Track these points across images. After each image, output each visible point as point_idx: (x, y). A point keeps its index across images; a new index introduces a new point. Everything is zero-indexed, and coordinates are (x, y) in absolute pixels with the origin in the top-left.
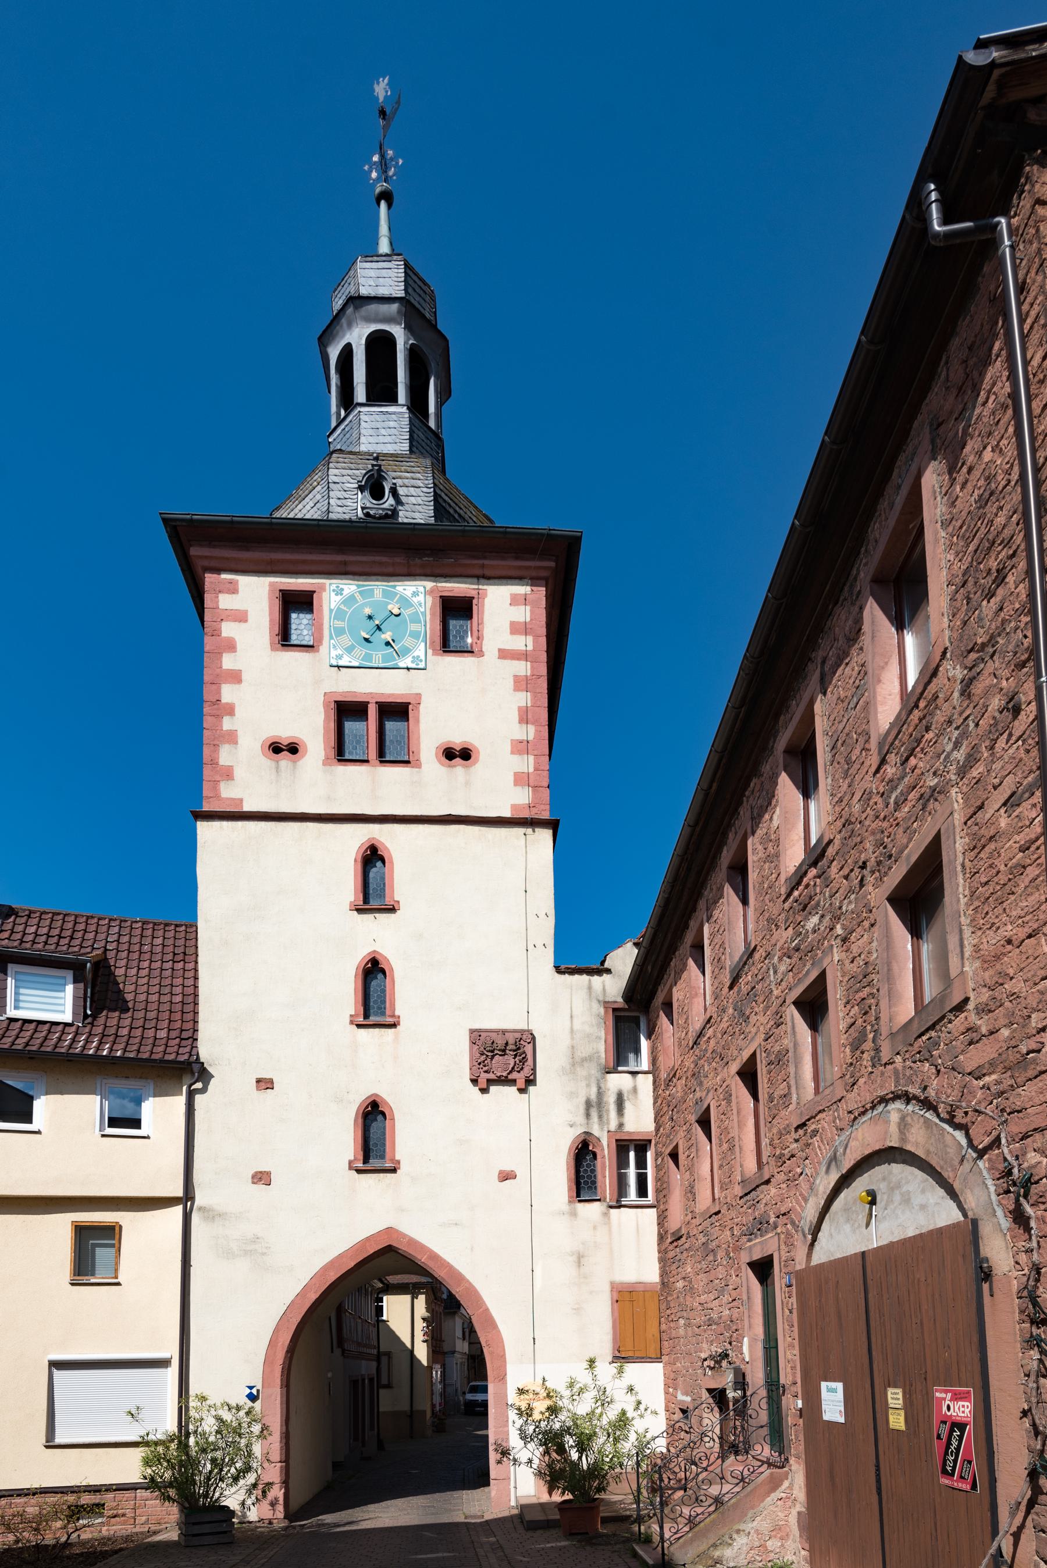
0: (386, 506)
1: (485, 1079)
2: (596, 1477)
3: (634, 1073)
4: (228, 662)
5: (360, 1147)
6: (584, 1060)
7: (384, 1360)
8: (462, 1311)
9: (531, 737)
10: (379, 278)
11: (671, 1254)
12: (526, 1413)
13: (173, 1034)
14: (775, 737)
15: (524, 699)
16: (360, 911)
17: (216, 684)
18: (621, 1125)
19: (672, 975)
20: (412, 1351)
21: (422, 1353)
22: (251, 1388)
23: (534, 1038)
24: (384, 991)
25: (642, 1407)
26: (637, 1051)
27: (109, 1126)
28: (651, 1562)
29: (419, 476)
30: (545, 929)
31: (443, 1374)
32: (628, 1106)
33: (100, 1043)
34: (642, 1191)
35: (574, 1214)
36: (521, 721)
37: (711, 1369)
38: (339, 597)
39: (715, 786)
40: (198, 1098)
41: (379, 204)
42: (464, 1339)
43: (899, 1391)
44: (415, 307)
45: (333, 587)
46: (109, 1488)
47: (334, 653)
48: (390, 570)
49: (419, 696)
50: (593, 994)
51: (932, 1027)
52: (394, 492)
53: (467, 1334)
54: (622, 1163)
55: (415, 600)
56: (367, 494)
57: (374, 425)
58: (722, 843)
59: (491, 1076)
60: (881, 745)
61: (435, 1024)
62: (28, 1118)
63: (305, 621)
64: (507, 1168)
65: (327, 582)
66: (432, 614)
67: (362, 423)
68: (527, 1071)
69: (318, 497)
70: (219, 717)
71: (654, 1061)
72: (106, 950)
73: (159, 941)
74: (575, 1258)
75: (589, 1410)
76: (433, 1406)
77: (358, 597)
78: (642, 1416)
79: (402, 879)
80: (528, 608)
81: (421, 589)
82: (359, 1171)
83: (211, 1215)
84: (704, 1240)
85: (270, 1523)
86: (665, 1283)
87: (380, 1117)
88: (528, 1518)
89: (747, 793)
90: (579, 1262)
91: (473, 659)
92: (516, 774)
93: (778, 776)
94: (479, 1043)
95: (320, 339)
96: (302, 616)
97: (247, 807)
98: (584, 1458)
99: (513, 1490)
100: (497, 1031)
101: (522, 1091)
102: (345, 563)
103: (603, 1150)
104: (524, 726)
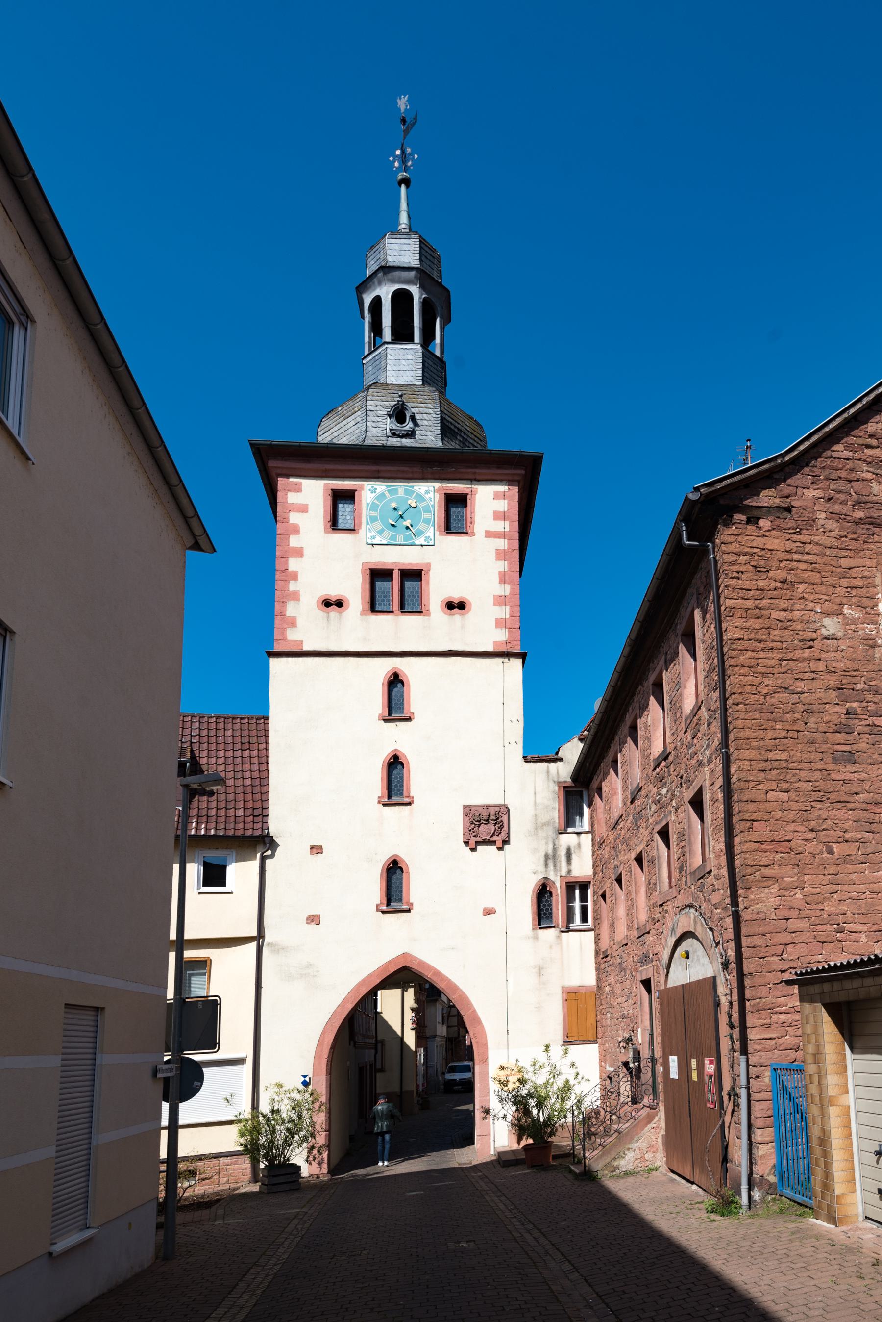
0: (407, 428)
1: (473, 843)
2: (549, 1126)
3: (579, 833)
4: (294, 541)
5: (384, 894)
6: (544, 825)
7: (379, 1046)
8: (444, 998)
9: (507, 593)
10: (402, 251)
11: (603, 966)
12: (504, 1084)
13: (249, 812)
15: (503, 566)
16: (386, 721)
17: (285, 557)
18: (569, 871)
20: (402, 1038)
21: (410, 1039)
22: (305, 1077)
23: (508, 810)
24: (402, 778)
25: (580, 1077)
26: (581, 815)
27: (204, 885)
28: (578, 1172)
29: (430, 405)
30: (517, 731)
31: (426, 1056)
33: (198, 823)
34: (584, 919)
35: (536, 938)
36: (500, 582)
37: (624, 1048)
38: (374, 494)
40: (268, 861)
41: (400, 186)
42: (443, 1024)
44: (428, 273)
45: (370, 487)
46: (200, 1158)
47: (369, 535)
48: (410, 475)
49: (429, 564)
50: (550, 777)
51: (702, 878)
52: (413, 418)
53: (446, 1019)
54: (570, 898)
55: (427, 496)
56: (394, 419)
57: (398, 357)
59: (478, 839)
60: (686, 720)
63: (348, 510)
64: (489, 905)
65: (365, 483)
66: (439, 506)
67: (389, 356)
68: (503, 835)
69: (359, 419)
70: (286, 582)
71: (592, 825)
72: (192, 743)
73: (229, 733)
74: (537, 970)
75: (545, 1080)
76: (418, 1086)
77: (386, 493)
78: (579, 1083)
79: (416, 697)
80: (506, 501)
81: (432, 489)
82: (384, 912)
83: (277, 949)
84: (619, 961)
85: (318, 1177)
86: (599, 987)
87: (399, 871)
88: (503, 1159)
90: (540, 973)
92: (495, 512)
93: (649, 697)
94: (470, 815)
95: (357, 288)
96: (346, 505)
97: (306, 648)
98: (541, 1114)
99: (492, 1143)
100: (482, 806)
101: (500, 849)
102: (378, 471)
104: (503, 585)
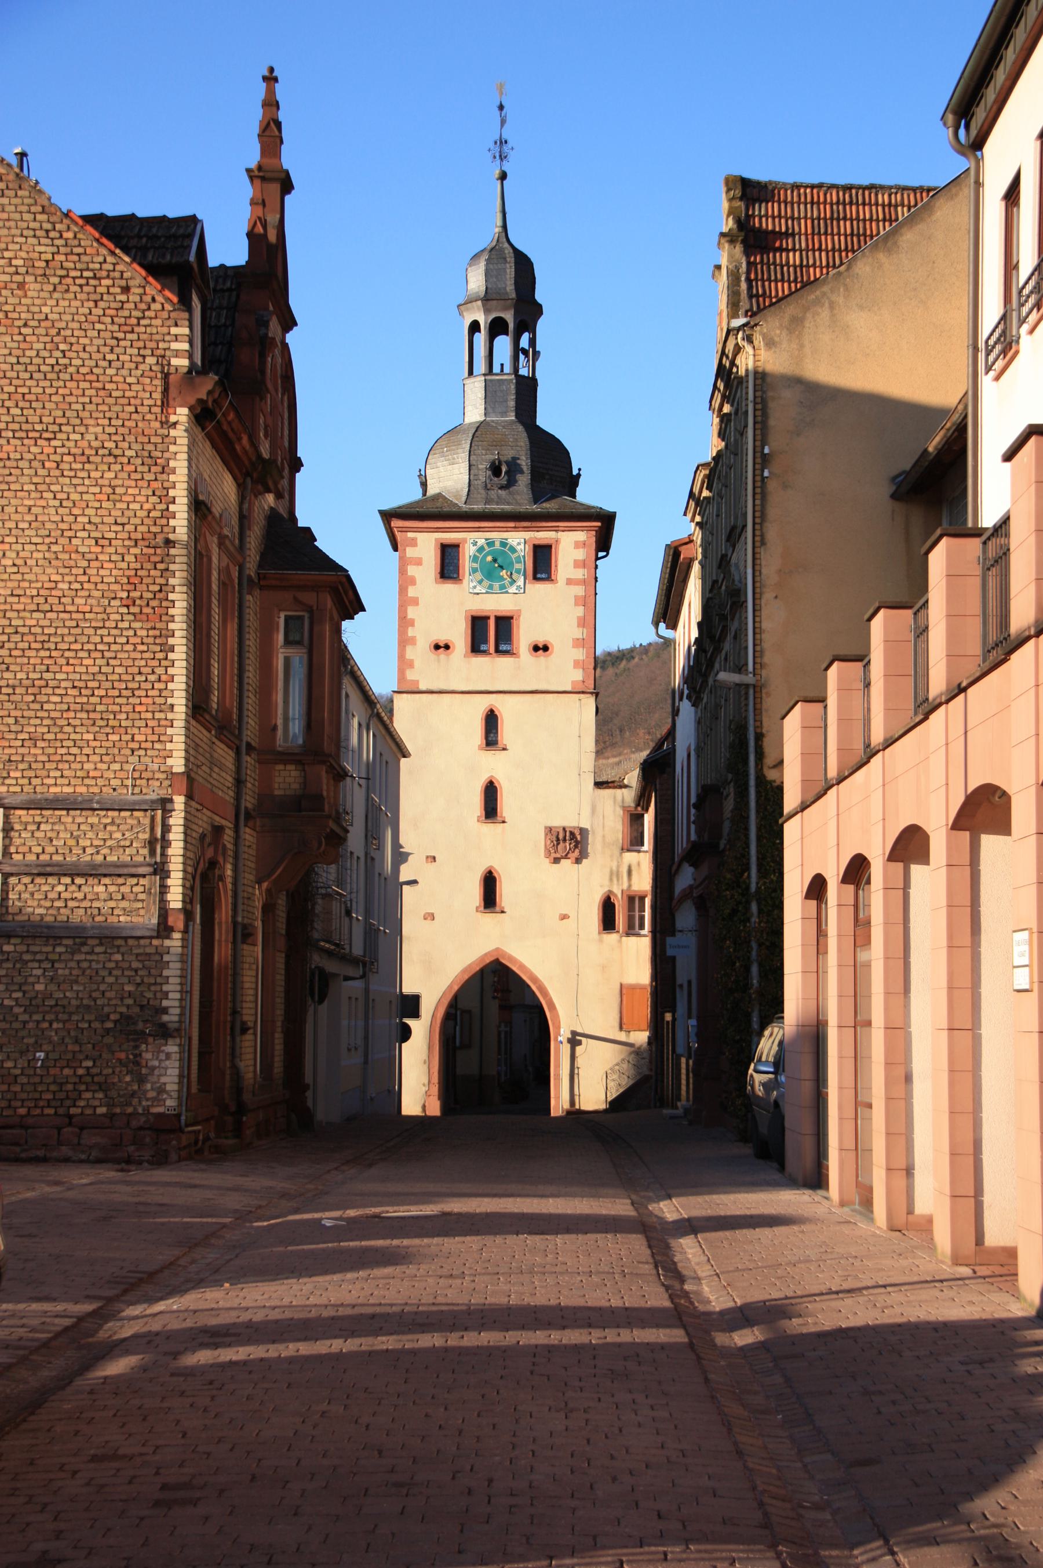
18: (630, 886)
47: (472, 585)
97: (422, 687)
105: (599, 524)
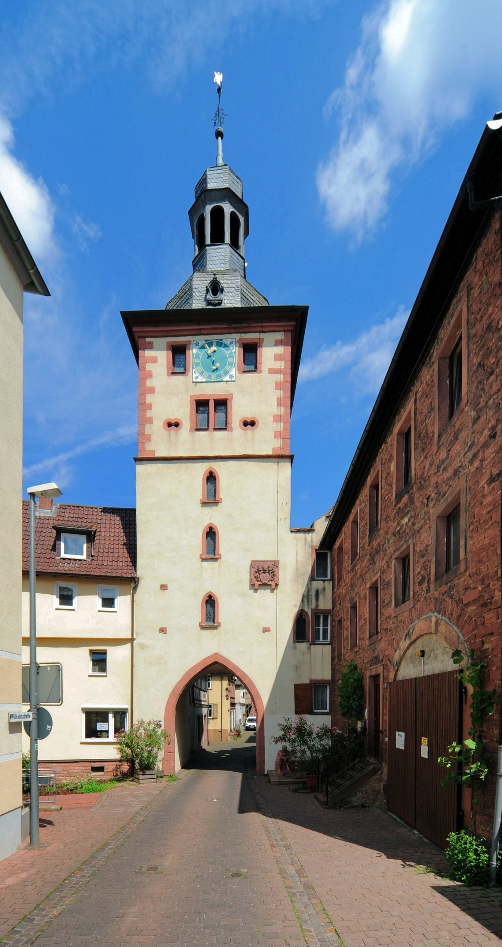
14: (394, 426)
18: (317, 606)
19: (343, 534)
32: (321, 597)
34: (325, 638)
35: (295, 648)
39: (366, 447)
43: (426, 739)
47: (195, 375)
58: (368, 474)
61: (236, 558)
62: (71, 604)
83: (143, 646)
89: (380, 451)
91: (256, 374)
97: (157, 455)
102: (200, 329)
103: (309, 617)
105: (294, 323)
